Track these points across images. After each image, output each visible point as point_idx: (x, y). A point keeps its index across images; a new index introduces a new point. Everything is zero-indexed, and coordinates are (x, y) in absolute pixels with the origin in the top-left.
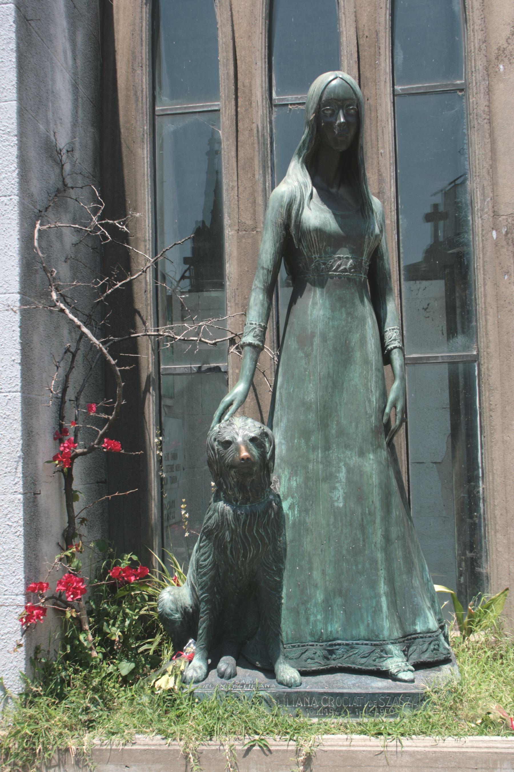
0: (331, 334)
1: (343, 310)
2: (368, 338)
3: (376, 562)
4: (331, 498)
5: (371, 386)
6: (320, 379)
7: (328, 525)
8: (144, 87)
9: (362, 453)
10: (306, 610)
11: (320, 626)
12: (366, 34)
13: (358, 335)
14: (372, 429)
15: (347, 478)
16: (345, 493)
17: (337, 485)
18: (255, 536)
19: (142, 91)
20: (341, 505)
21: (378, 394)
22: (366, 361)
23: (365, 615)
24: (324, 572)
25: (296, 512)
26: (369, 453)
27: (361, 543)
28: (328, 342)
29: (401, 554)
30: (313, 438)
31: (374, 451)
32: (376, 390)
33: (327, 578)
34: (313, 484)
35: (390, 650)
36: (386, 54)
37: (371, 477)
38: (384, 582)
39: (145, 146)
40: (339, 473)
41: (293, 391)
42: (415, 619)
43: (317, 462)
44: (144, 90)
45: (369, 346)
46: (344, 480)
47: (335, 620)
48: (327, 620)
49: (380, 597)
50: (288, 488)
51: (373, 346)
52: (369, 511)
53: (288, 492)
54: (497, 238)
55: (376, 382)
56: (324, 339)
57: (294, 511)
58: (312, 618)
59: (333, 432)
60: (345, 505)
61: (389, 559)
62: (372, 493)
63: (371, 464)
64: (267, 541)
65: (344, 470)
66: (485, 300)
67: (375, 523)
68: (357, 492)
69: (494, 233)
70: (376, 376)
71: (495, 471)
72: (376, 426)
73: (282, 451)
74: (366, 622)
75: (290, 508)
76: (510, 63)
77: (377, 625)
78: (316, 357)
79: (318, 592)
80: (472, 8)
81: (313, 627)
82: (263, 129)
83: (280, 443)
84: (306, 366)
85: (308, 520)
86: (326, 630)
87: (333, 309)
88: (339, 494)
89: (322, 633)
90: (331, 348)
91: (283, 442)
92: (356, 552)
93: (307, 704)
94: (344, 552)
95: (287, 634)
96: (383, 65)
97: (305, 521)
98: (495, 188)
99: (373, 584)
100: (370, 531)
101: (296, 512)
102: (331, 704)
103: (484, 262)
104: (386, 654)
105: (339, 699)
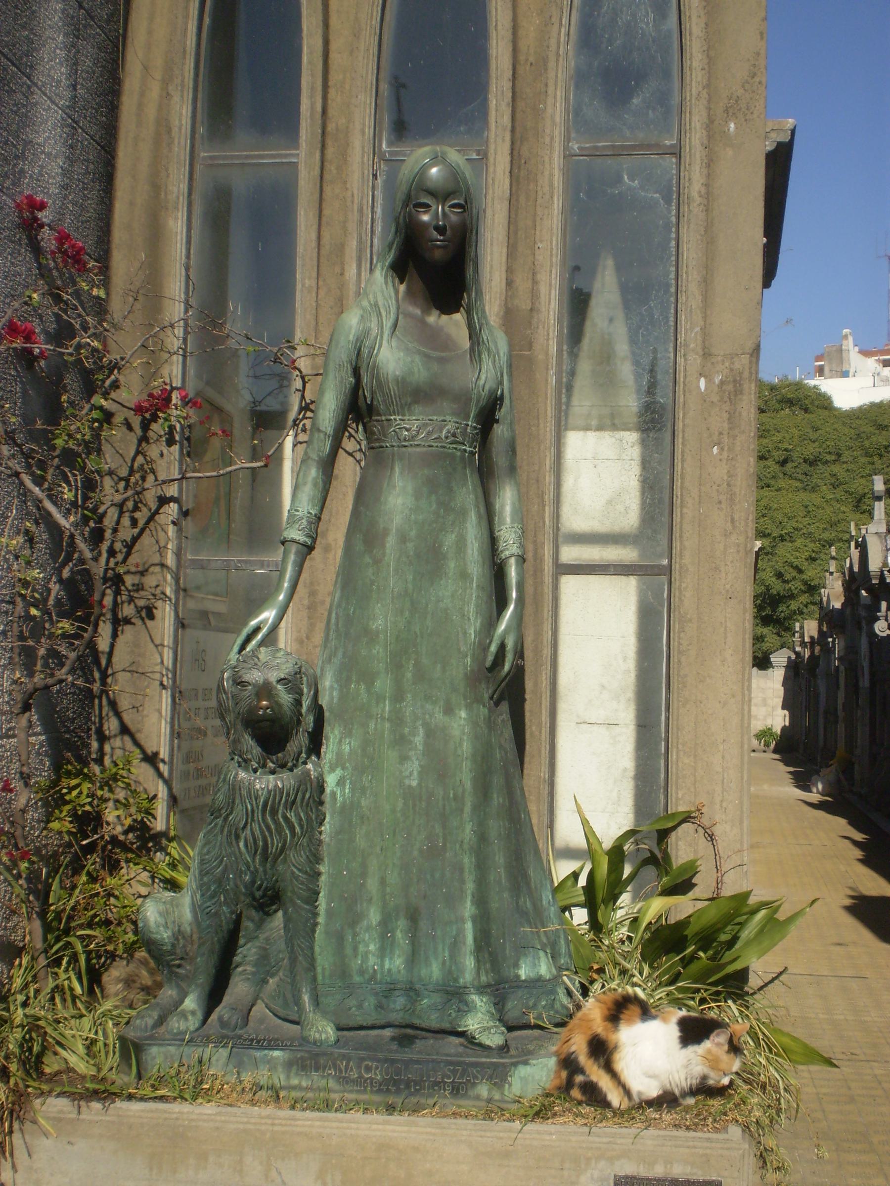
0: (413, 533)
1: (433, 497)
2: (469, 541)
3: (461, 870)
4: (401, 772)
5: (469, 612)
6: (393, 598)
7: (393, 811)
8: (184, 122)
9: (449, 710)
10: (355, 935)
11: (372, 960)
12: (531, 59)
13: (453, 536)
14: (466, 674)
15: (426, 744)
16: (421, 766)
17: (411, 753)
18: (280, 823)
19: (180, 129)
20: (414, 783)
21: (478, 624)
22: (464, 575)
23: (440, 947)
24: (383, 882)
25: (347, 791)
26: (460, 710)
27: (441, 840)
28: (408, 544)
29: (502, 861)
30: (378, 683)
31: (469, 707)
32: (476, 618)
33: (388, 890)
34: (374, 750)
35: (473, 1001)
36: (556, 94)
37: (461, 744)
38: (472, 901)
39: (180, 214)
40: (414, 736)
41: (354, 612)
42: (518, 960)
43: (383, 718)
44: (184, 128)
45: (469, 551)
46: (420, 747)
47: (397, 952)
48: (382, 952)
49: (463, 920)
50: (337, 754)
51: (476, 553)
52: (454, 794)
53: (337, 759)
54: (706, 389)
55: (477, 606)
56: (403, 539)
57: (344, 789)
58: (361, 948)
59: (409, 675)
60: (419, 784)
61: (482, 867)
62: (461, 767)
63: (461, 725)
64: (298, 829)
65: (421, 731)
66: (682, 483)
67: (462, 810)
68: (438, 765)
69: (702, 383)
70: (478, 597)
71: (680, 746)
72: (472, 671)
73: (332, 698)
74: (440, 959)
75: (338, 784)
76: (746, 120)
77: (456, 963)
78: (389, 566)
79: (372, 910)
80: (690, 34)
81: (362, 962)
82: (362, 198)
83: (332, 687)
84: (373, 578)
85: (363, 803)
86: (382, 966)
87: (417, 496)
88: (413, 767)
89: (375, 970)
90: (412, 553)
91: (336, 686)
92: (433, 852)
93: (341, 1072)
94: (416, 853)
95: (324, 969)
96: (550, 110)
97: (359, 803)
98: (709, 312)
99: (452, 901)
100: (455, 824)
101: (347, 791)
102: (375, 1074)
103: (684, 425)
104: (466, 1008)
105: (388, 1068)
